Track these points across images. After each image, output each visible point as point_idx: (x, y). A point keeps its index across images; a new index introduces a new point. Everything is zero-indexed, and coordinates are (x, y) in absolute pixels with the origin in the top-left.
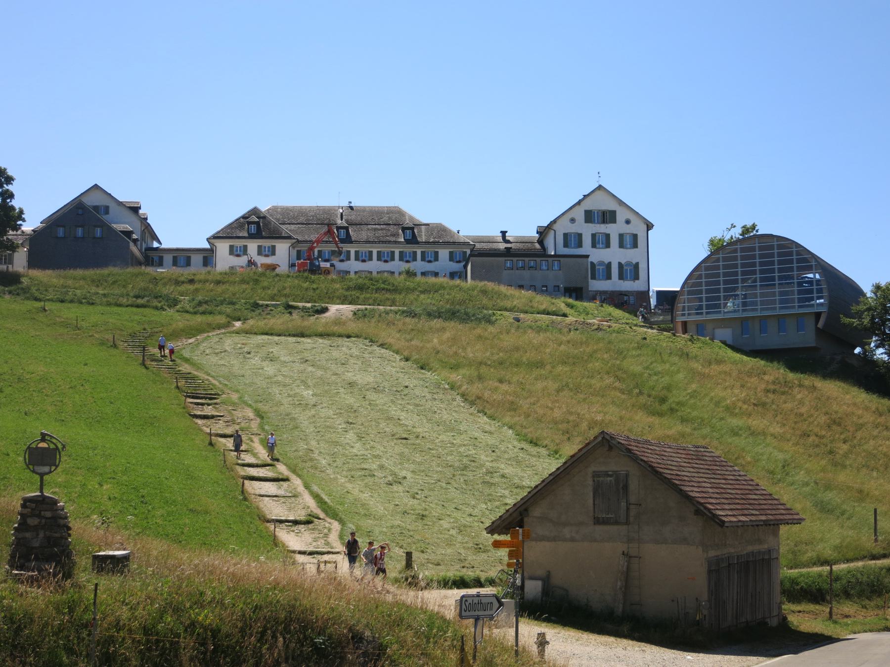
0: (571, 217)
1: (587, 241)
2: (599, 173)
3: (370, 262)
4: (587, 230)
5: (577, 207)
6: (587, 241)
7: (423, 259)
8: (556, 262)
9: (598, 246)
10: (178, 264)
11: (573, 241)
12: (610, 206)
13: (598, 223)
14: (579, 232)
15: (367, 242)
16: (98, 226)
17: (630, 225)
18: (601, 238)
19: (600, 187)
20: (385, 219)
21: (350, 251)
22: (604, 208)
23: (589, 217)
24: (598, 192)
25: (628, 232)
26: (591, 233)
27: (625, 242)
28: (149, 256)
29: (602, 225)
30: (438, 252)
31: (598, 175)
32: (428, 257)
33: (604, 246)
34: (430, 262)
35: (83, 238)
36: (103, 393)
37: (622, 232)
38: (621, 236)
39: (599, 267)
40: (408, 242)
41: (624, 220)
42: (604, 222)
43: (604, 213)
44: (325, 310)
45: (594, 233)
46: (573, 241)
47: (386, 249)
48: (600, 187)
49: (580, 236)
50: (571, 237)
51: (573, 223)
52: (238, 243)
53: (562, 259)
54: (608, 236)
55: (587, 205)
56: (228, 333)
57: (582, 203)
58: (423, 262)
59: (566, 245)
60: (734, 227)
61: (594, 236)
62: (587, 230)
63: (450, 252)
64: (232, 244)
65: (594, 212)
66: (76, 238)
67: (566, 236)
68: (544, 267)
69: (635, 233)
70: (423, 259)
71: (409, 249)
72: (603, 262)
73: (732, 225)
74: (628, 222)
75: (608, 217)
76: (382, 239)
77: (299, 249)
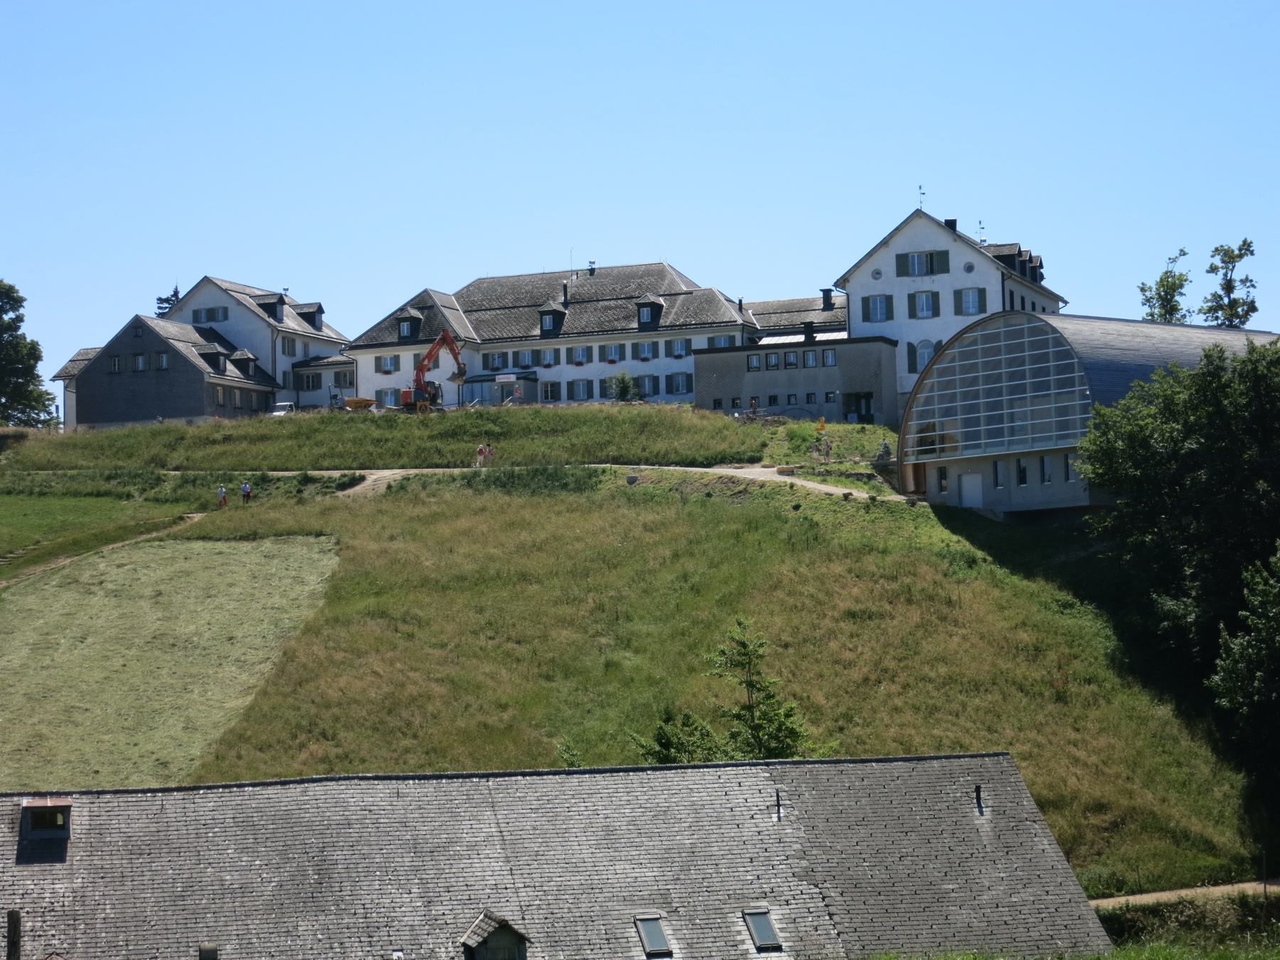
0: (872, 269)
1: (901, 307)
2: (920, 187)
3: (590, 364)
4: (901, 289)
5: (883, 251)
6: (901, 307)
7: (669, 353)
8: (811, 353)
9: (920, 314)
10: (976, 290)
11: (879, 309)
12: (941, 242)
13: (920, 275)
14: (888, 293)
15: (582, 334)
16: (141, 354)
17: (972, 274)
18: (922, 301)
19: (918, 213)
20: (508, 301)
21: (507, 353)
22: (929, 247)
23: (903, 265)
24: (919, 222)
25: (969, 285)
26: (907, 293)
27: (964, 305)
28: (302, 375)
29: (926, 278)
30: (690, 340)
31: (918, 192)
32: (611, 355)
33: (930, 313)
34: (612, 362)
35: (167, 369)
36: (637, 439)
37: (959, 287)
38: (958, 295)
39: (923, 350)
40: (643, 328)
41: (962, 266)
42: (931, 272)
43: (931, 255)
44: (363, 478)
45: (912, 292)
46: (879, 309)
47: (612, 342)
48: (918, 213)
49: (889, 299)
50: (875, 303)
51: (876, 279)
52: (387, 353)
53: (837, 347)
54: (935, 296)
55: (899, 246)
56: (154, 540)
57: (893, 242)
58: (669, 359)
59: (867, 317)
60: (1184, 254)
61: (912, 298)
62: (901, 289)
63: (709, 339)
64: (379, 355)
65: (913, 257)
66: (135, 371)
67: (865, 301)
68: (811, 362)
69: (981, 287)
70: (669, 353)
71: (646, 339)
72: (929, 341)
73: (1181, 251)
74: (969, 268)
75: (936, 263)
76: (607, 326)
77: (486, 352)
